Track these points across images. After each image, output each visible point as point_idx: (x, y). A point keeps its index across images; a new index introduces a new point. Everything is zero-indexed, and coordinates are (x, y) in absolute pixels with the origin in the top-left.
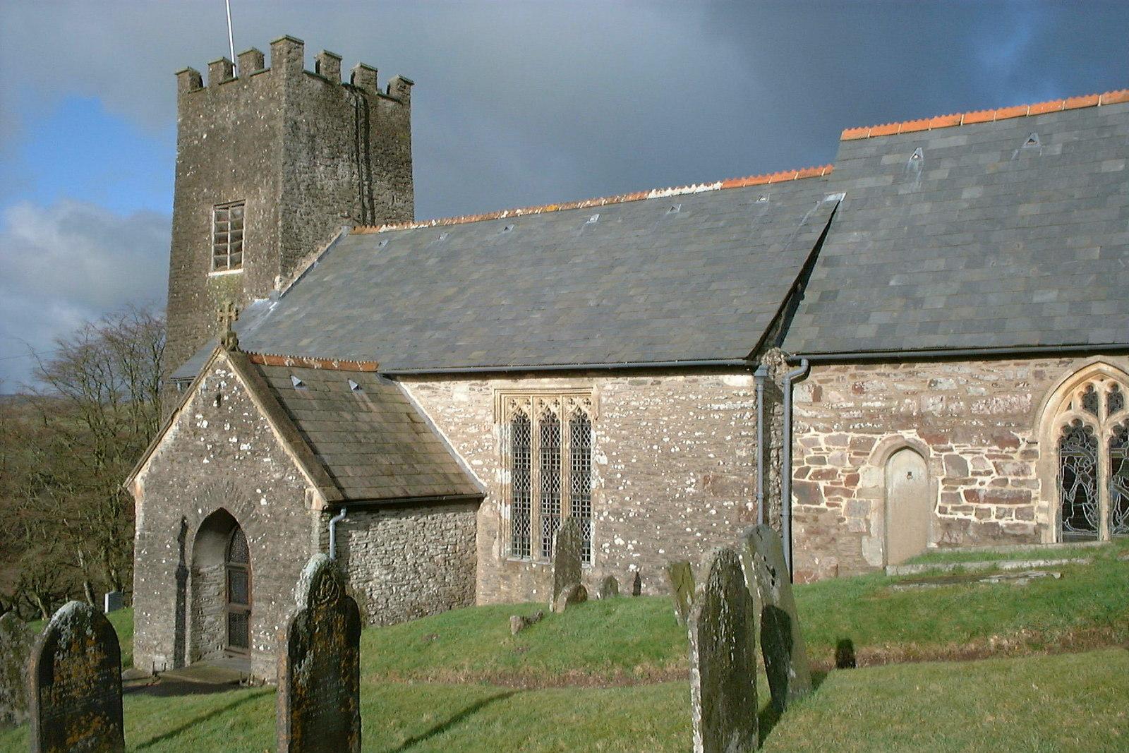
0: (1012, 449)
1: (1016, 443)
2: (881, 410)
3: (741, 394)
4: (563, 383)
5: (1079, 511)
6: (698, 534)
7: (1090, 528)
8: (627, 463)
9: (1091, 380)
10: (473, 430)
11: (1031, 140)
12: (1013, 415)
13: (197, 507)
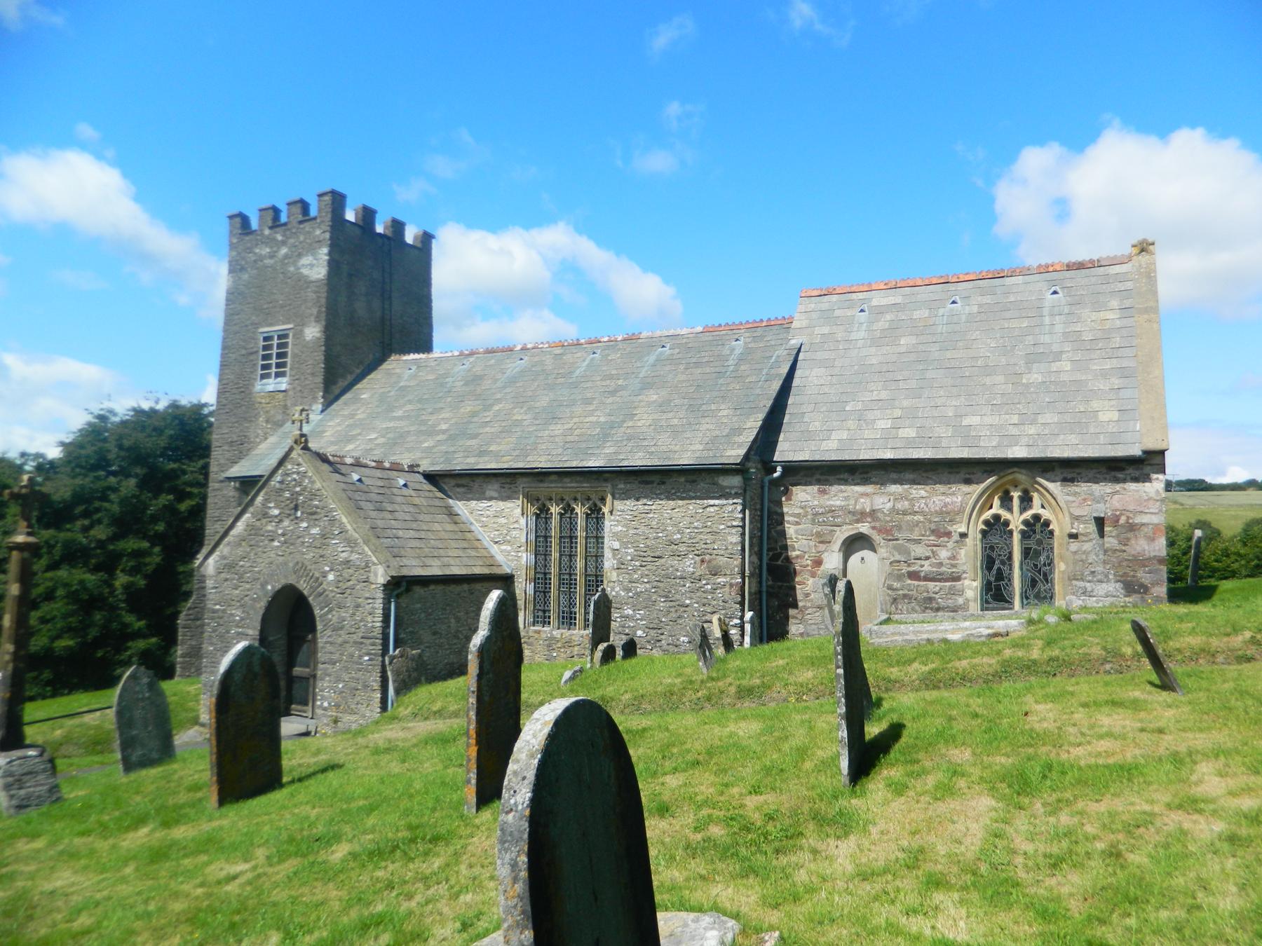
0: (946, 539)
1: (949, 534)
2: (841, 508)
3: (733, 492)
4: (581, 482)
5: (998, 588)
6: (696, 605)
7: (1007, 602)
8: (637, 548)
9: (1008, 486)
10: (503, 521)
11: (954, 302)
12: (948, 513)
13: (267, 583)
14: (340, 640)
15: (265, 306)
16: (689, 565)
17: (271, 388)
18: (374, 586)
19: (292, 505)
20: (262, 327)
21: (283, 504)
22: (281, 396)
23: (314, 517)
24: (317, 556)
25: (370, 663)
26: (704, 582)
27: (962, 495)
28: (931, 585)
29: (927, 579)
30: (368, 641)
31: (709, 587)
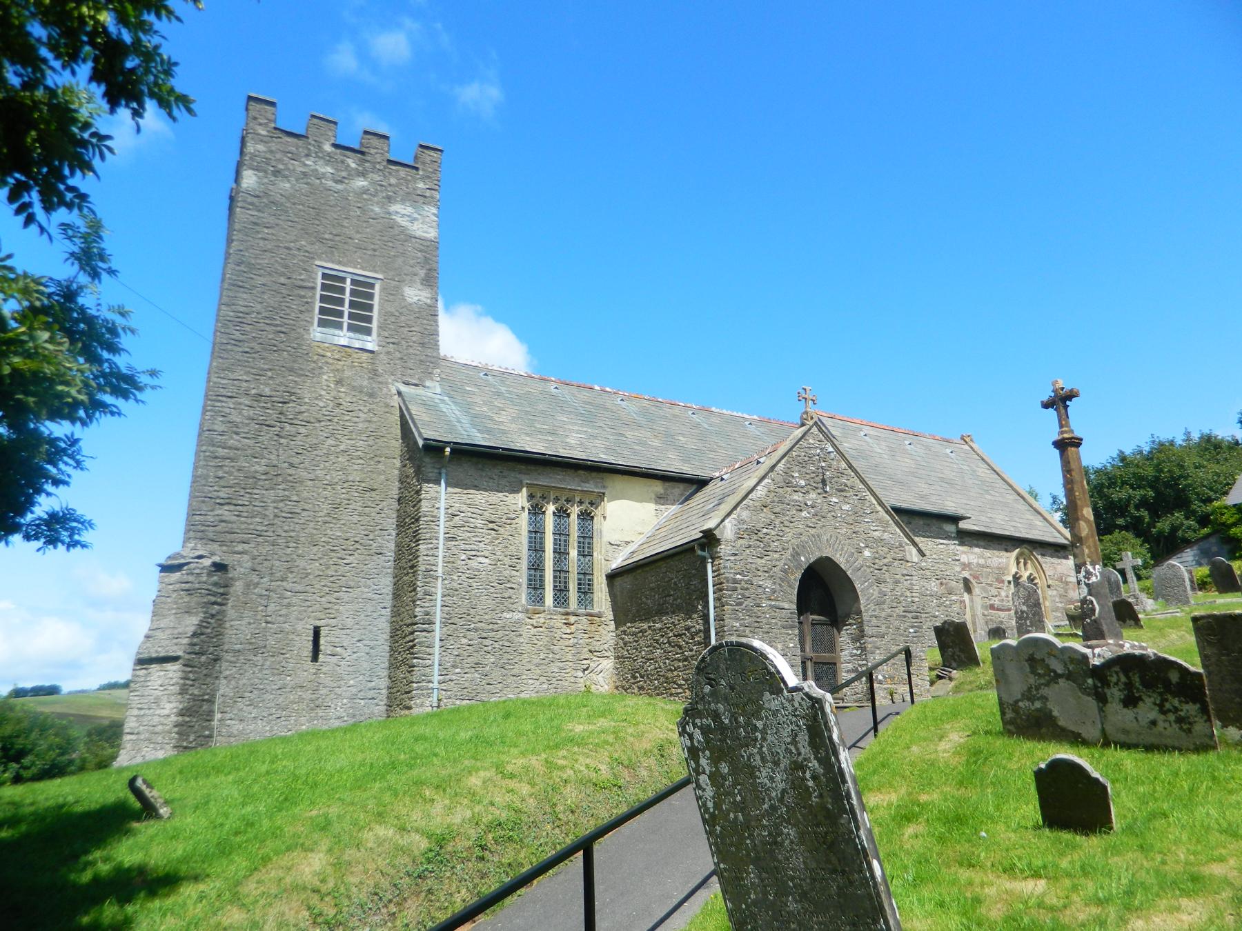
14: (883, 614)
15: (327, 236)
16: (934, 586)
17: (343, 341)
18: (909, 564)
19: (819, 479)
20: (321, 260)
21: (808, 477)
22: (365, 356)
23: (844, 494)
24: (850, 531)
25: (914, 635)
26: (909, 600)
27: (1007, 560)
28: (1000, 613)
29: (998, 610)
30: (910, 615)
31: (948, 602)
